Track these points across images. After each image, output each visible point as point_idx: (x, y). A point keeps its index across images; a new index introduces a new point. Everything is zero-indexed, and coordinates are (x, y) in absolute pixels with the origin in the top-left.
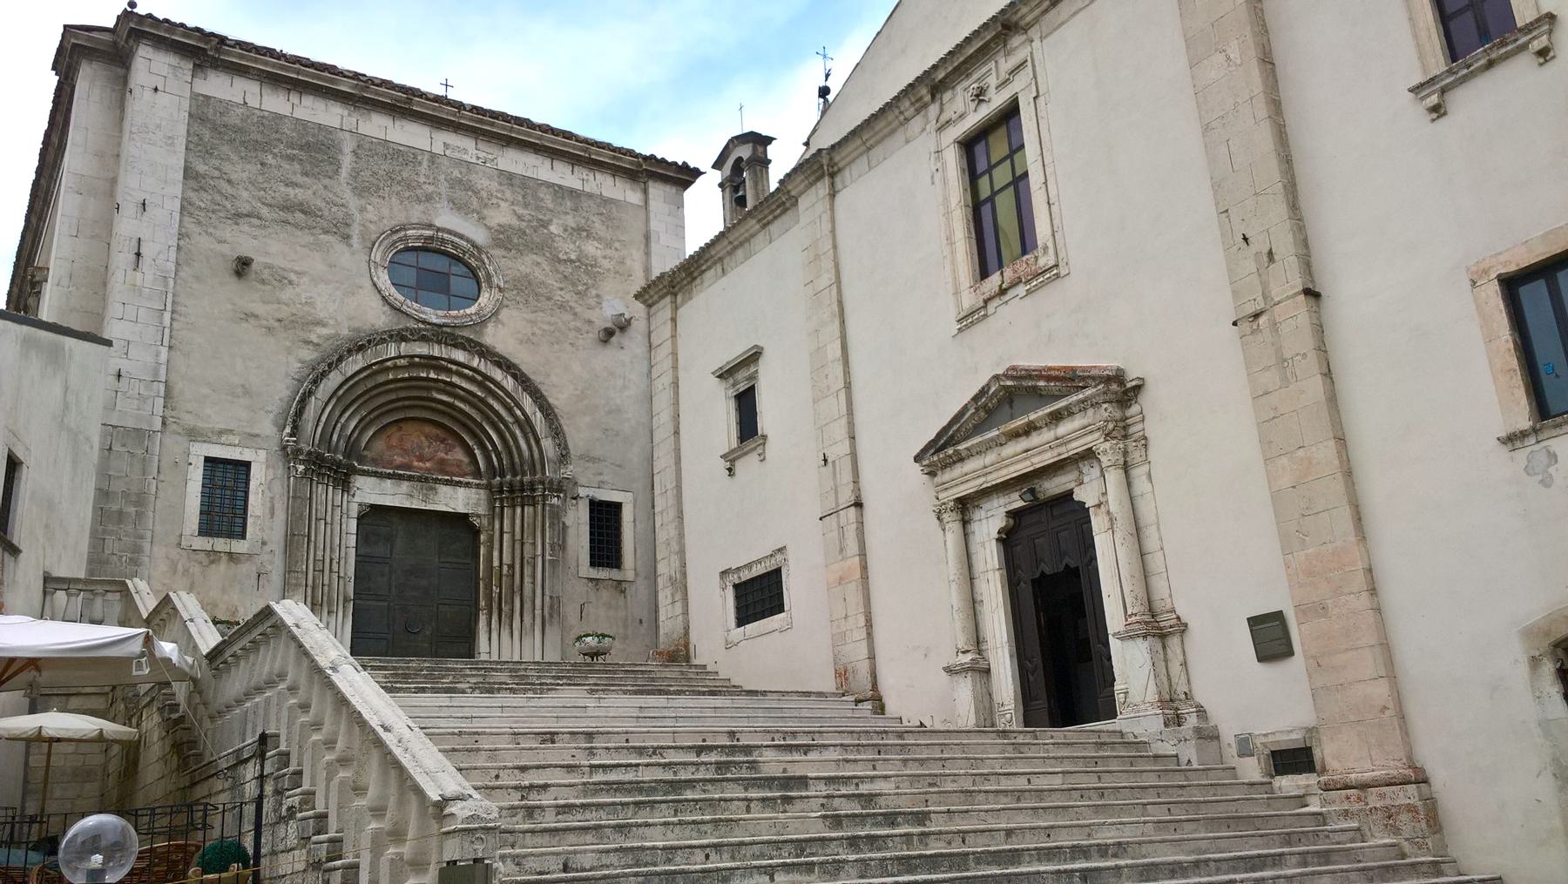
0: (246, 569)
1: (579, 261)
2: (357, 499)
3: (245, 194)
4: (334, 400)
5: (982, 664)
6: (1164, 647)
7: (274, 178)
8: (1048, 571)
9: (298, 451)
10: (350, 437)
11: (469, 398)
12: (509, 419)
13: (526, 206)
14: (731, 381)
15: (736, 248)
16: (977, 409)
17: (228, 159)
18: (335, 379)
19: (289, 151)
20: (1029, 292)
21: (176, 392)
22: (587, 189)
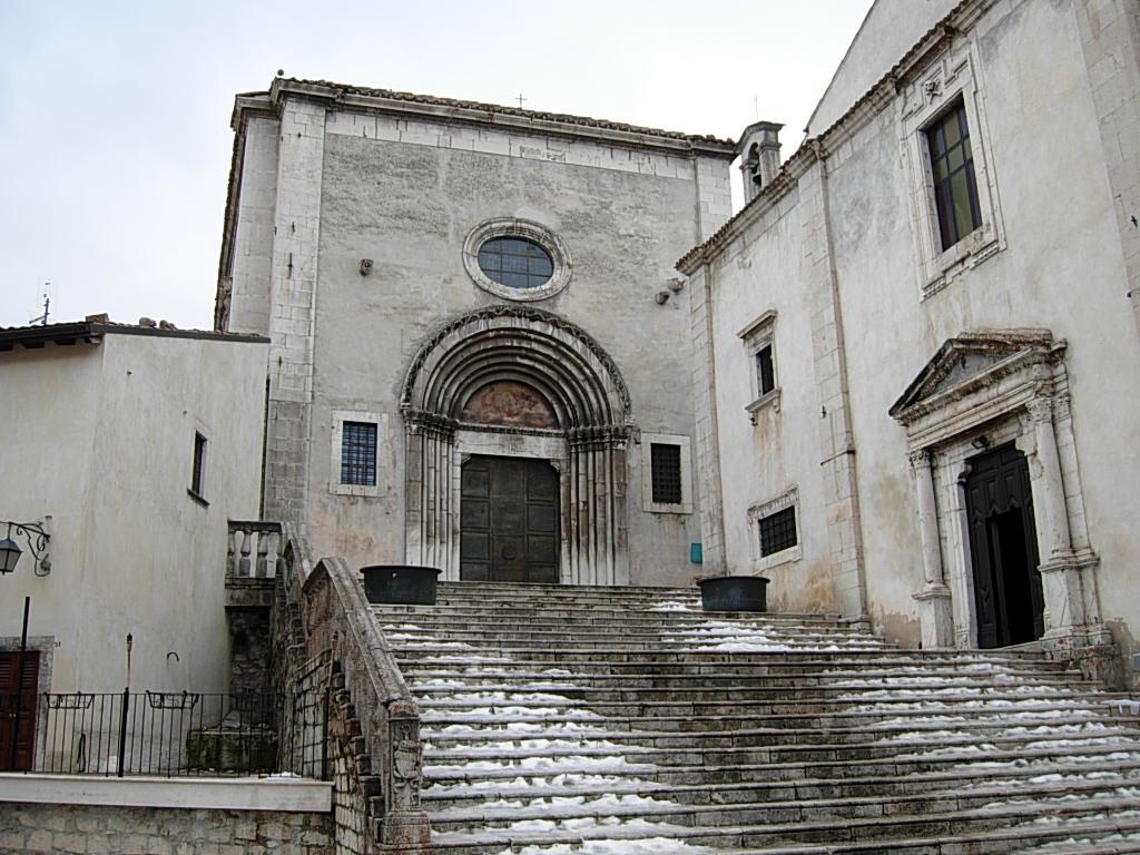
0: (379, 508)
2: (460, 450)
3: (366, 209)
4: (438, 370)
5: (944, 592)
6: (1081, 578)
8: (999, 511)
9: (411, 414)
12: (580, 377)
13: (590, 192)
14: (752, 341)
16: (937, 369)
18: (438, 352)
20: (977, 264)
22: (643, 171)
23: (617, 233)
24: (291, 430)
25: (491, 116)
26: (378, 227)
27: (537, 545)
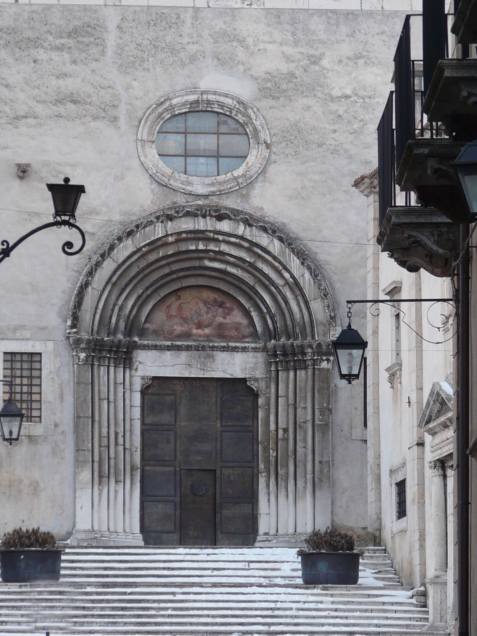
0: (45, 449)
1: (356, 95)
2: (140, 373)
3: (22, 96)
10: (128, 317)
11: (239, 262)
12: (279, 282)
13: (296, 43)
18: (108, 266)
23: (330, 95)
27: (232, 478)
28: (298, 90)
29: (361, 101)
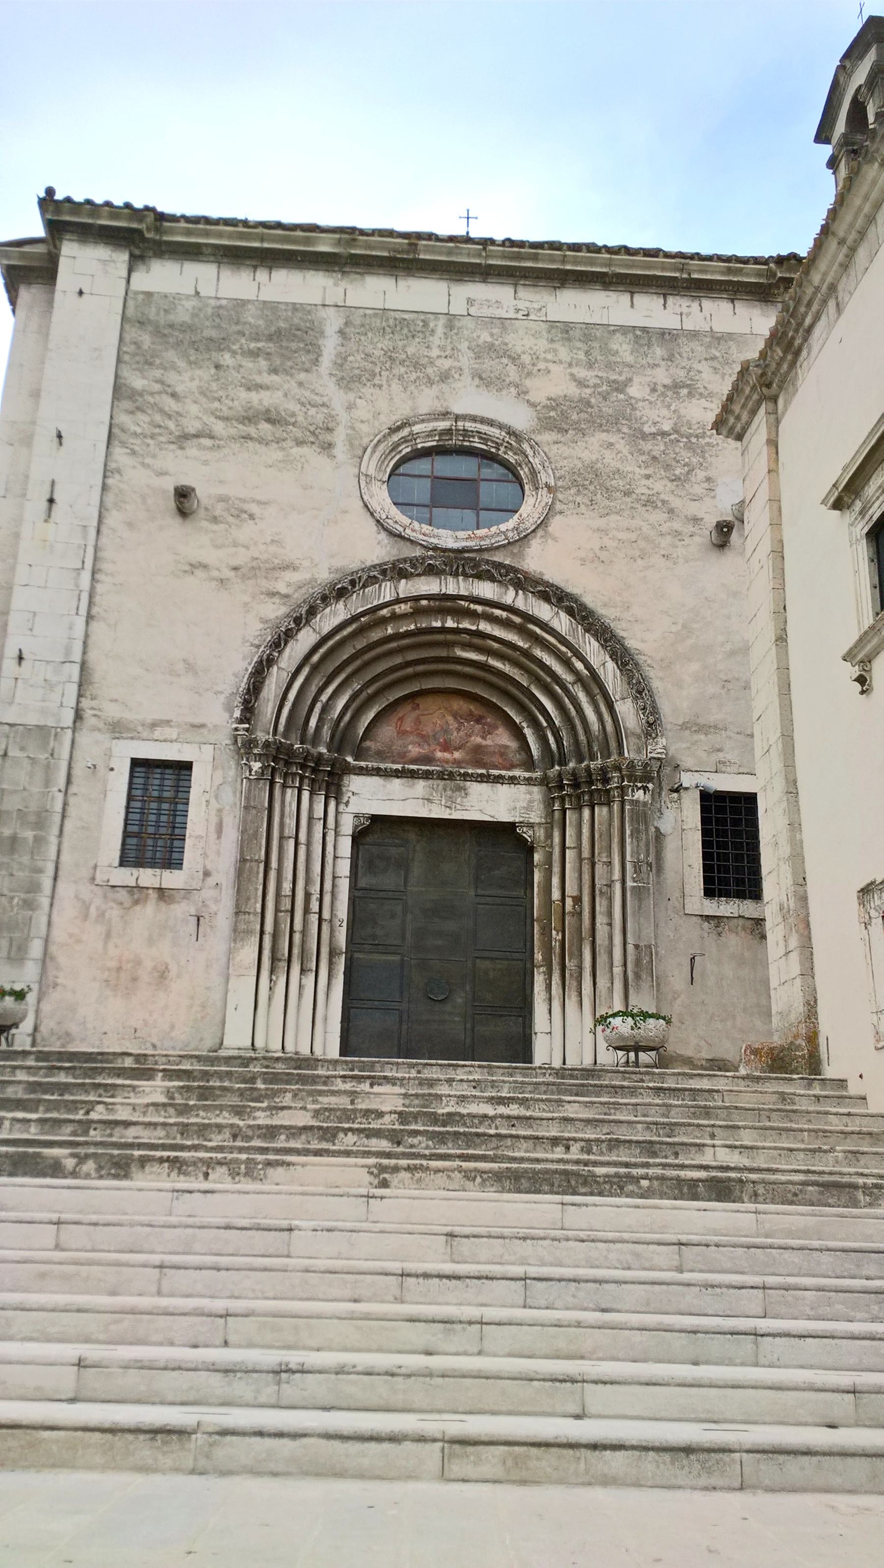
0: (181, 910)
1: (676, 431)
3: (194, 409)
4: (306, 671)
7: (232, 382)
12: (568, 677)
13: (590, 366)
14: (858, 505)
15: (853, 250)
17: (174, 367)
18: (306, 639)
19: (253, 345)
21: (97, 677)
22: (688, 325)
24: (31, 775)
25: (413, 247)
26: (212, 437)
28: (594, 422)
29: (685, 440)
